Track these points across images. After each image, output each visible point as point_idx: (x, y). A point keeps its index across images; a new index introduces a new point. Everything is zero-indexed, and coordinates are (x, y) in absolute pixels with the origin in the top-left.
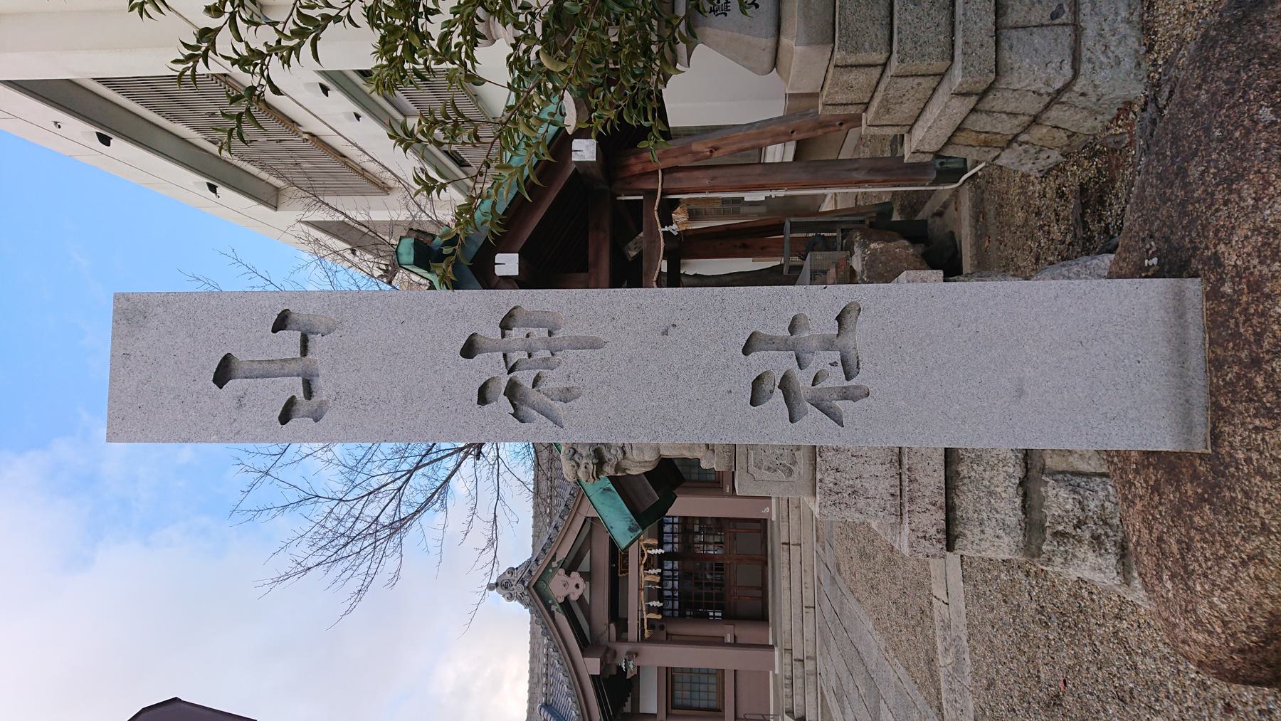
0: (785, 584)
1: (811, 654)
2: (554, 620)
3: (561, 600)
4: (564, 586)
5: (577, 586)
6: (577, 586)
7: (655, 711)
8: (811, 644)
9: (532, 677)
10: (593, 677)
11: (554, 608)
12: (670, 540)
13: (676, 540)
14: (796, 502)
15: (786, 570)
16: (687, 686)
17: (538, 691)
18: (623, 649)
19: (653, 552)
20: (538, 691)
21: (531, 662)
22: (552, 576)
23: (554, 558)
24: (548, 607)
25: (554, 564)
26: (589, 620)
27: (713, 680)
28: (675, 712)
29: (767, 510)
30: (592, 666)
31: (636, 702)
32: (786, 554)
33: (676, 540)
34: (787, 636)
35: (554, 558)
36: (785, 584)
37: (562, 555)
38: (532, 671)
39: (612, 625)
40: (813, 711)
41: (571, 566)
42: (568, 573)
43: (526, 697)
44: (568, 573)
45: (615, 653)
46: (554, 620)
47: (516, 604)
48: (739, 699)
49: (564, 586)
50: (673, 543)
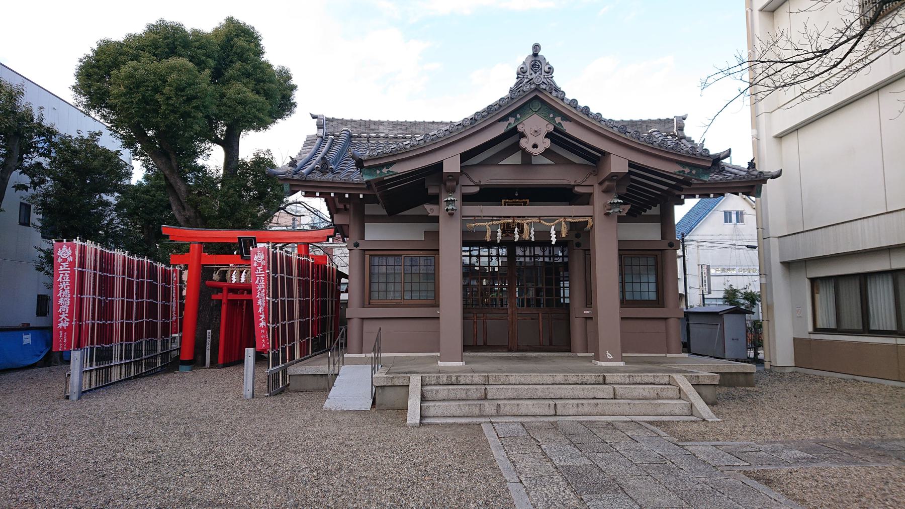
0: (559, 377)
1: (503, 410)
2: (499, 121)
3: (520, 128)
4: (535, 131)
5: (535, 146)
6: (535, 146)
7: (368, 237)
8: (515, 411)
9: (375, 123)
10: (440, 164)
11: (512, 120)
12: (527, 253)
13: (528, 260)
14: (664, 394)
15: (575, 379)
16: (399, 269)
17: (363, 129)
18: (456, 197)
19: (553, 232)
20: (363, 129)
21: (388, 122)
22: (545, 118)
23: (566, 118)
24: (512, 114)
25: (558, 120)
26: (482, 164)
27: (653, 296)
28: (367, 257)
29: (610, 356)
30: (452, 165)
31: (376, 219)
32: (593, 380)
33: (547, 260)
34: (503, 379)
35: (566, 118)
36: (559, 377)
37: (569, 128)
38: (381, 123)
39: (477, 189)
40: (440, 412)
41: (557, 137)
42: (548, 135)
43: (356, 118)
44: (548, 135)
45: (452, 191)
46: (499, 121)
47: (512, 81)
48: (374, 322)
49: (535, 131)
50: (525, 256)
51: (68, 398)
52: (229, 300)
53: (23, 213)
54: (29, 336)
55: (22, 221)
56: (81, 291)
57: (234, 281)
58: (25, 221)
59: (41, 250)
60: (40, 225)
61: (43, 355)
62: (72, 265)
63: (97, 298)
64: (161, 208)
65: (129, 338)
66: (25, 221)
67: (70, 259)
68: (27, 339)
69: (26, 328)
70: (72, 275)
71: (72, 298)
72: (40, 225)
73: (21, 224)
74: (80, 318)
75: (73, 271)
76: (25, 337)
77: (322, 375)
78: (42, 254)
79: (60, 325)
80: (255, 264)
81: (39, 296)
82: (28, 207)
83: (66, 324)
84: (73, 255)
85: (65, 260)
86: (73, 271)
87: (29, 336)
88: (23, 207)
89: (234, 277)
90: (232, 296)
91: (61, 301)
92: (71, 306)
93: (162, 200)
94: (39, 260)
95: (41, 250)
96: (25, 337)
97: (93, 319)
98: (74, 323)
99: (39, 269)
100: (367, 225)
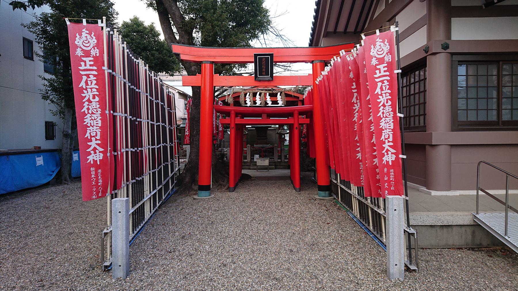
51: (107, 269)
52: (236, 124)
53: (26, 47)
54: (41, 158)
55: (27, 55)
56: (114, 108)
57: (249, 104)
58: (29, 55)
59: (45, 79)
60: (42, 54)
61: (55, 174)
62: (98, 61)
63: (129, 117)
64: (139, 50)
65: (154, 168)
66: (29, 55)
67: (95, 52)
68: (40, 161)
69: (38, 151)
70: (100, 77)
71: (103, 115)
72: (42, 54)
73: (25, 57)
74: (115, 149)
75: (101, 72)
76: (37, 159)
77: (442, 226)
78: (46, 83)
79: (91, 158)
80: (374, 62)
81: (46, 123)
82: (30, 43)
83: (99, 157)
84: (99, 45)
85: (87, 54)
86: (101, 72)
87: (41, 158)
88: (26, 42)
89: (248, 100)
90: (239, 121)
91: (88, 120)
92: (103, 128)
93: (139, 43)
94: (44, 88)
95: (45, 79)
96: (37, 159)
97: (127, 147)
98: (108, 154)
99: (45, 98)
100: (453, 20)
